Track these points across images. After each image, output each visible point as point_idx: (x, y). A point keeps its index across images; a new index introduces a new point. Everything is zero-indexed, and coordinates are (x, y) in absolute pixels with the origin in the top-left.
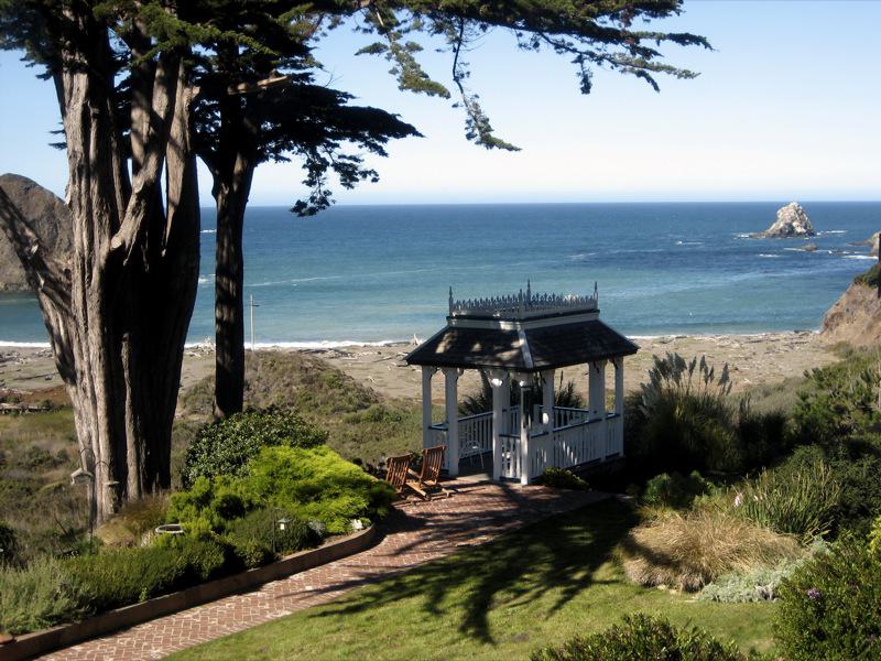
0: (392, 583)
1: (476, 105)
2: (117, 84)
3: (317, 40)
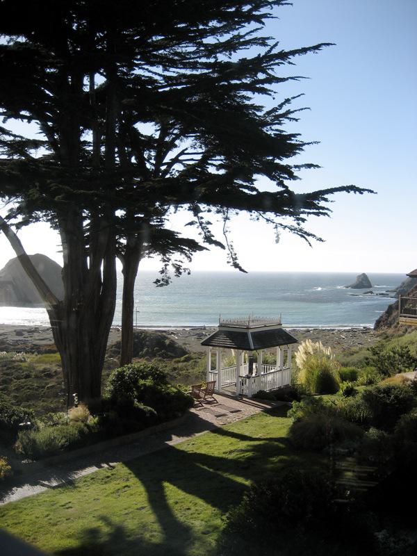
0: (241, 40)
1: (270, 95)
2: (84, 225)
3: (168, 216)
